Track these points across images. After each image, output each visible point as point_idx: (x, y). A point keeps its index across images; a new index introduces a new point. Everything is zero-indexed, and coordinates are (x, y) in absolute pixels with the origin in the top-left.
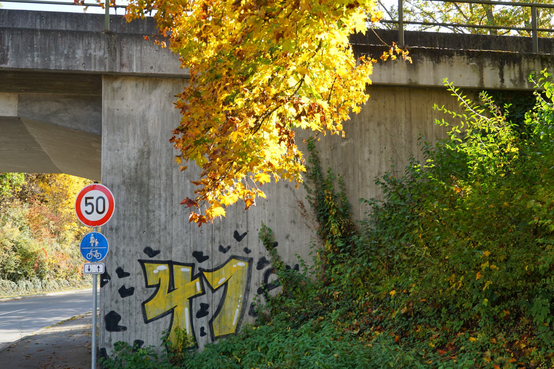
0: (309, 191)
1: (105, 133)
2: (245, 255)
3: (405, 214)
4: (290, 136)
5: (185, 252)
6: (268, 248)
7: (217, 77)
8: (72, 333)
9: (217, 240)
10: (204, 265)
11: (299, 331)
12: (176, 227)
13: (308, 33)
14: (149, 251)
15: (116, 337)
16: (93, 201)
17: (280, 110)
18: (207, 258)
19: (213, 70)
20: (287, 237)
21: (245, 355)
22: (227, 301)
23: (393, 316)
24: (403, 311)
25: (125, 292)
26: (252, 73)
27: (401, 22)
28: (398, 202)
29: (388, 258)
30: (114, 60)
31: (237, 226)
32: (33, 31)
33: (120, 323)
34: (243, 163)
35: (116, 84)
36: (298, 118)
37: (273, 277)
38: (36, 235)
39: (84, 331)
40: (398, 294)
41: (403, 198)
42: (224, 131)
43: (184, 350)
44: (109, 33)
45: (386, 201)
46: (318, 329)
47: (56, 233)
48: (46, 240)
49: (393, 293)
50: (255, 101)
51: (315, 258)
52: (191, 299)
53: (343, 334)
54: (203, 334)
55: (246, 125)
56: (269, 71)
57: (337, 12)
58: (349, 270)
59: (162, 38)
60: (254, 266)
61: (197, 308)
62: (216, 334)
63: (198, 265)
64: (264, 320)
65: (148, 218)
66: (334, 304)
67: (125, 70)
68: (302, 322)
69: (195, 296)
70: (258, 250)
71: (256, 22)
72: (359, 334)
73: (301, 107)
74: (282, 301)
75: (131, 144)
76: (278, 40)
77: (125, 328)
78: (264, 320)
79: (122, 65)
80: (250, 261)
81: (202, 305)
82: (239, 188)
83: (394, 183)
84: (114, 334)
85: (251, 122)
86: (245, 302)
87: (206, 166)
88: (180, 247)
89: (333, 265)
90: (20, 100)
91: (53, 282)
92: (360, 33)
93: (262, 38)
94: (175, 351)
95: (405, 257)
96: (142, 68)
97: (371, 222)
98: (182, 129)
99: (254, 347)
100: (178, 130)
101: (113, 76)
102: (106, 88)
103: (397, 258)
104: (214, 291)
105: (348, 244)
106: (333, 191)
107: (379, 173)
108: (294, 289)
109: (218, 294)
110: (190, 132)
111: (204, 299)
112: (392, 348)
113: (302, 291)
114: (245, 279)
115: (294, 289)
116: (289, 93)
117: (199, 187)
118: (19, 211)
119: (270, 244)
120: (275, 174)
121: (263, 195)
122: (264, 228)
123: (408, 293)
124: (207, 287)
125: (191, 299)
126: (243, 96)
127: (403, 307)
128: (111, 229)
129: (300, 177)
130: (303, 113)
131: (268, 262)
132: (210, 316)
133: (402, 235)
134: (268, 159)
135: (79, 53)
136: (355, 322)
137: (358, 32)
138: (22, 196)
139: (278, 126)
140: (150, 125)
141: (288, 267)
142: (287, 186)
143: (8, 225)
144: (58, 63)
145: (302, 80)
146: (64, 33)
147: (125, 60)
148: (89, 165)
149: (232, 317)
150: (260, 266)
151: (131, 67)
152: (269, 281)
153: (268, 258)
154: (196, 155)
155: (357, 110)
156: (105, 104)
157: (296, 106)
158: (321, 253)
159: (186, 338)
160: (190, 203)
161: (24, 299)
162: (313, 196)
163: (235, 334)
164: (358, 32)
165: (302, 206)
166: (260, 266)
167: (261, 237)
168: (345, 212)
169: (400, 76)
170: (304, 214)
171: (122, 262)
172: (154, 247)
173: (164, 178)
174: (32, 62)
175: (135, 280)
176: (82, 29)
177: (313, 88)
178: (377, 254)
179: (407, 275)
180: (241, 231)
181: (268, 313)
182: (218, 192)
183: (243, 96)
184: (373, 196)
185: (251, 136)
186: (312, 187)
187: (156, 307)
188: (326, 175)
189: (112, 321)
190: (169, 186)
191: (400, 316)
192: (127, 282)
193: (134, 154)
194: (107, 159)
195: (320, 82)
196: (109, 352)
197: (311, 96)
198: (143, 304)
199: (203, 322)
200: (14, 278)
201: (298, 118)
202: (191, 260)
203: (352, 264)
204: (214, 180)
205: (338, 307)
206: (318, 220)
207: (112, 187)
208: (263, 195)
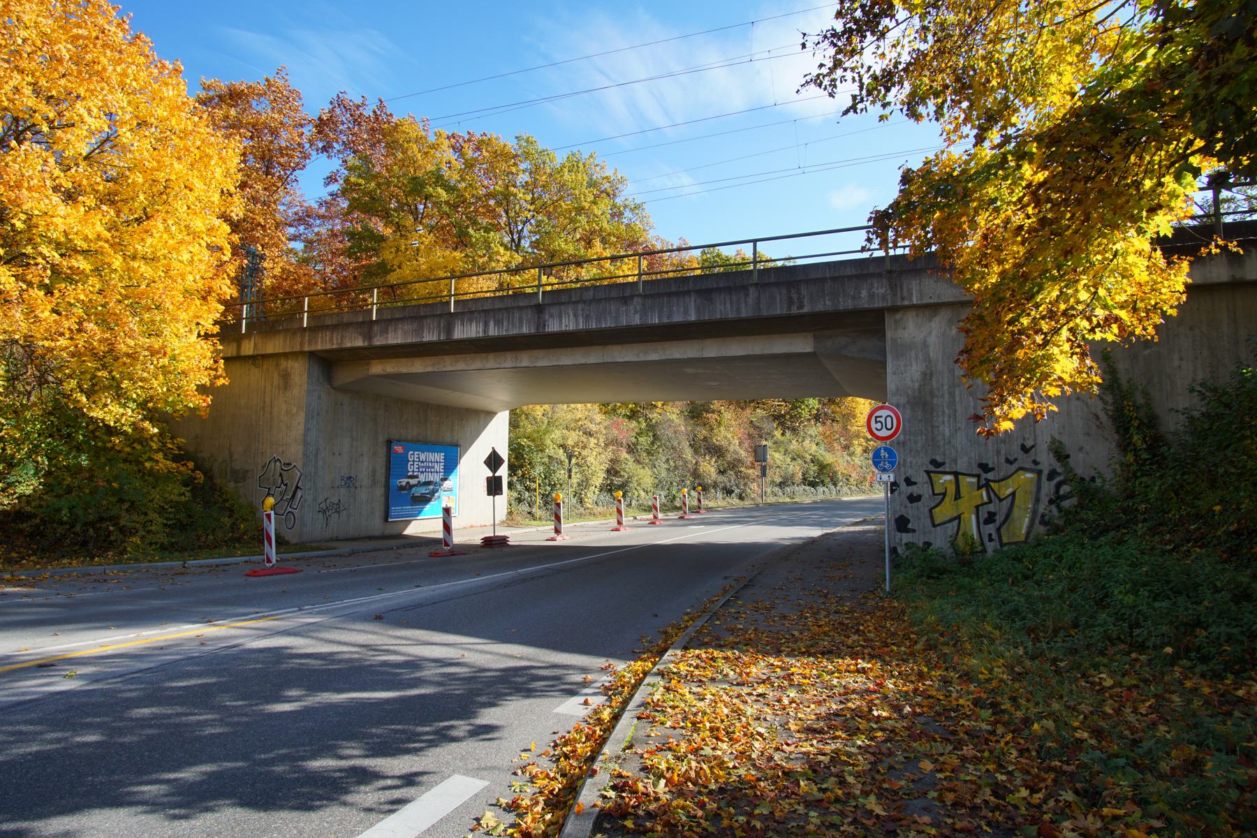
0: (1105, 403)
1: (889, 360)
2: (1033, 467)
3: (1231, 423)
4: (1085, 349)
5: (970, 464)
6: (1059, 460)
7: (1000, 300)
8: (864, 532)
9: (1003, 452)
10: (990, 476)
11: (1097, 543)
12: (960, 439)
13: (1100, 245)
14: (934, 462)
15: (906, 538)
16: (882, 420)
17: (1071, 324)
18: (993, 469)
19: (996, 294)
20: (1081, 449)
21: (1036, 562)
22: (1015, 510)
23: (1219, 533)
24: (1232, 528)
25: (913, 499)
26: (1038, 292)
27: (1218, 215)
28: (1221, 410)
29: (1210, 471)
30: (895, 295)
31: (1024, 439)
32: (824, 280)
33: (910, 526)
34: (1031, 379)
35: (898, 316)
36: (1092, 330)
37: (1065, 489)
38: (830, 449)
39: (875, 531)
40: (1224, 510)
41: (1228, 406)
42: (1011, 349)
43: (972, 553)
44: (890, 272)
45: (1204, 410)
46: (1121, 542)
47: (846, 447)
48: (839, 453)
49: (1218, 508)
50: (1043, 318)
51: (1114, 470)
52: (977, 507)
53: (1153, 548)
54: (991, 540)
55: (1034, 342)
56: (1057, 287)
57: (1135, 219)
58: (1159, 483)
59: (944, 270)
60: (1044, 477)
61: (983, 515)
62: (1005, 540)
63: (984, 476)
64: (1057, 530)
65: (933, 432)
66: (1140, 517)
67: (906, 303)
68: (1101, 534)
69: (982, 505)
70: (1047, 461)
71: (1042, 243)
72: (1173, 550)
73: (1094, 319)
74: (1076, 512)
75: (914, 367)
76: (1066, 256)
77: (914, 531)
78: (1057, 530)
79: (903, 299)
80: (1039, 473)
81: (989, 513)
82: (1027, 403)
83: (1215, 390)
84: (904, 535)
85: (1039, 339)
86: (1034, 512)
87: (991, 384)
88: (965, 459)
89: (1137, 478)
90: (815, 337)
91: (845, 489)
92: (1165, 236)
93: (1048, 258)
94: (964, 554)
95: (1233, 470)
96: (921, 298)
97: (1186, 432)
98: (967, 351)
99: (1046, 556)
100: (962, 352)
101: (895, 309)
102: (889, 321)
103: (1221, 470)
104: (1001, 500)
105: (1155, 455)
106: (1134, 402)
107: (1194, 380)
108: (1091, 501)
109: (1006, 504)
110: (974, 353)
111: (991, 508)
112: (1220, 567)
113: (1099, 502)
114: (1034, 489)
115: (1091, 501)
116: (1080, 307)
117: (987, 404)
118: (815, 430)
119: (1061, 455)
120: (1066, 388)
121: (1055, 408)
122: (1054, 440)
123: (1238, 509)
124: (994, 497)
125: (977, 507)
126: (1029, 315)
127: (1232, 523)
128: (898, 443)
129: (1095, 388)
130: (1098, 325)
131: (1059, 474)
132: (998, 523)
133: (1228, 446)
134: (1058, 373)
135: (864, 293)
136: (1168, 537)
137: (1162, 234)
138: (817, 418)
139: (1069, 340)
140: (931, 349)
141: (1083, 479)
142: (1078, 399)
143: (807, 441)
144: (846, 304)
145: (1096, 293)
146: (850, 277)
147: (905, 294)
148: (875, 390)
149: (1022, 523)
150: (1050, 478)
151: (911, 300)
152: (1061, 492)
153: (1059, 470)
154: (981, 375)
155: (1173, 312)
156: (889, 334)
157: (1089, 319)
158: (1122, 464)
159: (973, 543)
160: (978, 418)
161: (822, 502)
162: (1109, 408)
163: (1026, 542)
164: (1162, 234)
165: (1097, 417)
166: (1050, 478)
167: (1050, 449)
168: (1151, 422)
169: (1220, 273)
170: (1100, 426)
171: (910, 472)
172: (939, 459)
173: (946, 396)
174: (824, 305)
175: (922, 489)
176: (865, 272)
177: (1108, 299)
178: (1193, 466)
179: (1237, 489)
180: (1029, 444)
181: (1061, 523)
182: (1006, 407)
183: (1029, 315)
184: (1187, 405)
185: (1040, 353)
186: (1109, 398)
187: (944, 512)
188: (1125, 386)
189: (902, 524)
190: (952, 404)
191: (1229, 534)
192: (914, 490)
193: (917, 376)
194: (892, 383)
195: (1117, 291)
196: (900, 550)
197: (1105, 307)
198: (930, 510)
199: (991, 529)
200: (813, 484)
201: (1092, 330)
202: (977, 471)
203: (1161, 477)
204: (1002, 396)
205: (1145, 520)
206: (1117, 432)
207: (898, 406)
208: (1055, 408)
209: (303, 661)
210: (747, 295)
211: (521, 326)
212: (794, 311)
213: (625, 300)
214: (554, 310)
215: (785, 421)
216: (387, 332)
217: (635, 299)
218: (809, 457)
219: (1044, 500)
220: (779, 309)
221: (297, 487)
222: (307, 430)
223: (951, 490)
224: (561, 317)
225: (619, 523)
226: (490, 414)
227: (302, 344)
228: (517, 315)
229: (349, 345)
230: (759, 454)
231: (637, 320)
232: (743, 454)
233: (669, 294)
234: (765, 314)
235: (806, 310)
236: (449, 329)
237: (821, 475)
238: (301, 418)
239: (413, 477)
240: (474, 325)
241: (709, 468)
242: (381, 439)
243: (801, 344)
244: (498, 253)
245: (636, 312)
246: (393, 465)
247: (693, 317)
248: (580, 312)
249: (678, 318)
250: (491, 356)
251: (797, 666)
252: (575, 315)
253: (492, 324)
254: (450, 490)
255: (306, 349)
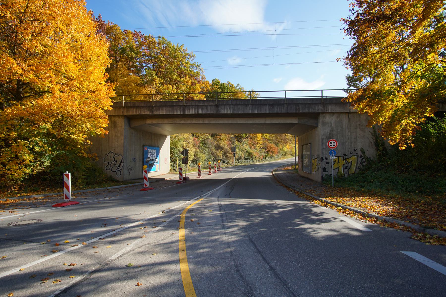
10: (346, 157)
15: (325, 173)
35: (324, 115)
37: (364, 160)
61: (345, 167)
63: (345, 157)
70: (360, 153)
80: (358, 156)
86: (357, 166)
111: (346, 165)
119: (363, 152)
124: (347, 162)
135: (316, 108)
144: (311, 111)
149: (354, 168)
150: (360, 157)
171: (326, 156)
174: (306, 111)
180: (355, 149)
186: (374, 138)
193: (329, 131)
199: (346, 170)
200: (246, 159)
202: (343, 156)
209: (49, 231)
210: (284, 106)
211: (211, 111)
212: (297, 112)
213: (247, 105)
214: (223, 107)
215: (239, 139)
216: (159, 110)
217: (250, 105)
218: (245, 150)
219: (359, 163)
220: (293, 111)
221: (121, 162)
222: (124, 142)
223: (337, 160)
224: (225, 109)
225: (210, 172)
226: (166, 136)
227: (123, 112)
228: (209, 107)
229: (144, 114)
230: (233, 149)
231: (250, 112)
232: (229, 149)
233: (261, 105)
234: (289, 112)
235: (301, 112)
236: (184, 110)
237: (249, 156)
238: (122, 137)
239: (150, 158)
240: (193, 110)
241: (220, 154)
242: (142, 145)
243: (294, 121)
244: (155, 78)
245: (250, 109)
246: (144, 154)
247: (268, 112)
248: (231, 108)
249: (263, 112)
250: (194, 119)
251: (357, 199)
252: (230, 109)
253: (200, 110)
254: (157, 162)
255: (125, 114)
